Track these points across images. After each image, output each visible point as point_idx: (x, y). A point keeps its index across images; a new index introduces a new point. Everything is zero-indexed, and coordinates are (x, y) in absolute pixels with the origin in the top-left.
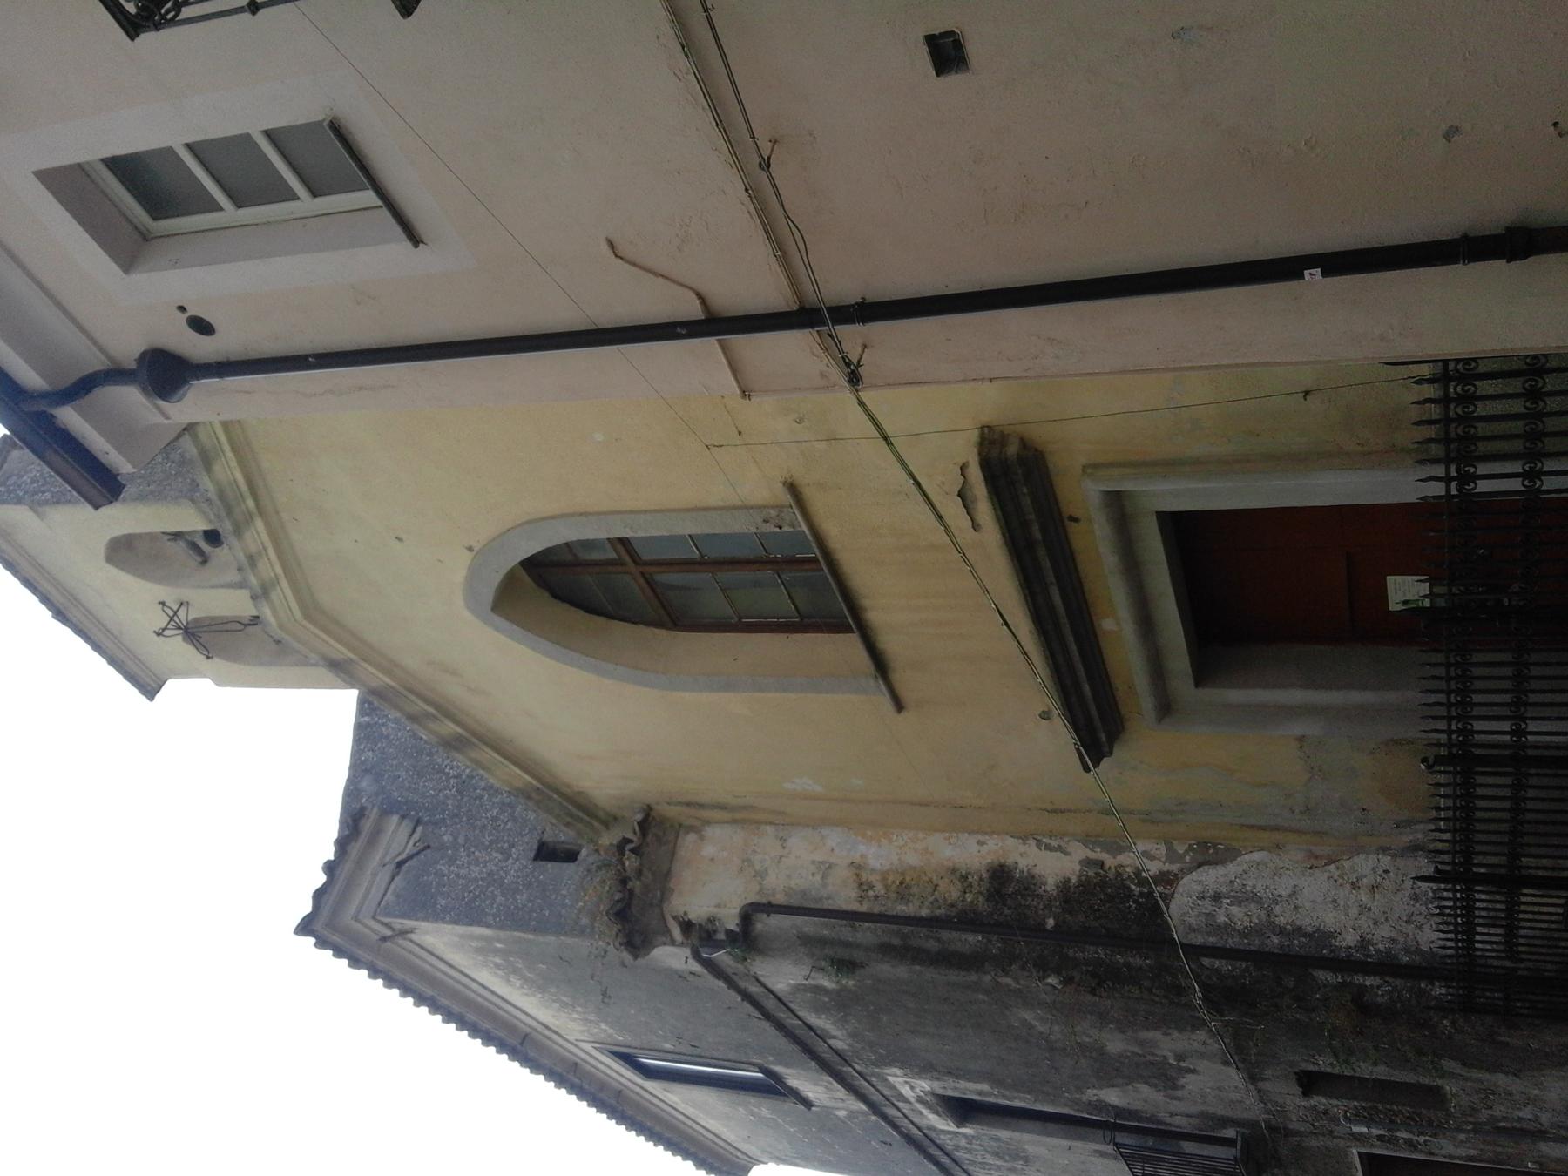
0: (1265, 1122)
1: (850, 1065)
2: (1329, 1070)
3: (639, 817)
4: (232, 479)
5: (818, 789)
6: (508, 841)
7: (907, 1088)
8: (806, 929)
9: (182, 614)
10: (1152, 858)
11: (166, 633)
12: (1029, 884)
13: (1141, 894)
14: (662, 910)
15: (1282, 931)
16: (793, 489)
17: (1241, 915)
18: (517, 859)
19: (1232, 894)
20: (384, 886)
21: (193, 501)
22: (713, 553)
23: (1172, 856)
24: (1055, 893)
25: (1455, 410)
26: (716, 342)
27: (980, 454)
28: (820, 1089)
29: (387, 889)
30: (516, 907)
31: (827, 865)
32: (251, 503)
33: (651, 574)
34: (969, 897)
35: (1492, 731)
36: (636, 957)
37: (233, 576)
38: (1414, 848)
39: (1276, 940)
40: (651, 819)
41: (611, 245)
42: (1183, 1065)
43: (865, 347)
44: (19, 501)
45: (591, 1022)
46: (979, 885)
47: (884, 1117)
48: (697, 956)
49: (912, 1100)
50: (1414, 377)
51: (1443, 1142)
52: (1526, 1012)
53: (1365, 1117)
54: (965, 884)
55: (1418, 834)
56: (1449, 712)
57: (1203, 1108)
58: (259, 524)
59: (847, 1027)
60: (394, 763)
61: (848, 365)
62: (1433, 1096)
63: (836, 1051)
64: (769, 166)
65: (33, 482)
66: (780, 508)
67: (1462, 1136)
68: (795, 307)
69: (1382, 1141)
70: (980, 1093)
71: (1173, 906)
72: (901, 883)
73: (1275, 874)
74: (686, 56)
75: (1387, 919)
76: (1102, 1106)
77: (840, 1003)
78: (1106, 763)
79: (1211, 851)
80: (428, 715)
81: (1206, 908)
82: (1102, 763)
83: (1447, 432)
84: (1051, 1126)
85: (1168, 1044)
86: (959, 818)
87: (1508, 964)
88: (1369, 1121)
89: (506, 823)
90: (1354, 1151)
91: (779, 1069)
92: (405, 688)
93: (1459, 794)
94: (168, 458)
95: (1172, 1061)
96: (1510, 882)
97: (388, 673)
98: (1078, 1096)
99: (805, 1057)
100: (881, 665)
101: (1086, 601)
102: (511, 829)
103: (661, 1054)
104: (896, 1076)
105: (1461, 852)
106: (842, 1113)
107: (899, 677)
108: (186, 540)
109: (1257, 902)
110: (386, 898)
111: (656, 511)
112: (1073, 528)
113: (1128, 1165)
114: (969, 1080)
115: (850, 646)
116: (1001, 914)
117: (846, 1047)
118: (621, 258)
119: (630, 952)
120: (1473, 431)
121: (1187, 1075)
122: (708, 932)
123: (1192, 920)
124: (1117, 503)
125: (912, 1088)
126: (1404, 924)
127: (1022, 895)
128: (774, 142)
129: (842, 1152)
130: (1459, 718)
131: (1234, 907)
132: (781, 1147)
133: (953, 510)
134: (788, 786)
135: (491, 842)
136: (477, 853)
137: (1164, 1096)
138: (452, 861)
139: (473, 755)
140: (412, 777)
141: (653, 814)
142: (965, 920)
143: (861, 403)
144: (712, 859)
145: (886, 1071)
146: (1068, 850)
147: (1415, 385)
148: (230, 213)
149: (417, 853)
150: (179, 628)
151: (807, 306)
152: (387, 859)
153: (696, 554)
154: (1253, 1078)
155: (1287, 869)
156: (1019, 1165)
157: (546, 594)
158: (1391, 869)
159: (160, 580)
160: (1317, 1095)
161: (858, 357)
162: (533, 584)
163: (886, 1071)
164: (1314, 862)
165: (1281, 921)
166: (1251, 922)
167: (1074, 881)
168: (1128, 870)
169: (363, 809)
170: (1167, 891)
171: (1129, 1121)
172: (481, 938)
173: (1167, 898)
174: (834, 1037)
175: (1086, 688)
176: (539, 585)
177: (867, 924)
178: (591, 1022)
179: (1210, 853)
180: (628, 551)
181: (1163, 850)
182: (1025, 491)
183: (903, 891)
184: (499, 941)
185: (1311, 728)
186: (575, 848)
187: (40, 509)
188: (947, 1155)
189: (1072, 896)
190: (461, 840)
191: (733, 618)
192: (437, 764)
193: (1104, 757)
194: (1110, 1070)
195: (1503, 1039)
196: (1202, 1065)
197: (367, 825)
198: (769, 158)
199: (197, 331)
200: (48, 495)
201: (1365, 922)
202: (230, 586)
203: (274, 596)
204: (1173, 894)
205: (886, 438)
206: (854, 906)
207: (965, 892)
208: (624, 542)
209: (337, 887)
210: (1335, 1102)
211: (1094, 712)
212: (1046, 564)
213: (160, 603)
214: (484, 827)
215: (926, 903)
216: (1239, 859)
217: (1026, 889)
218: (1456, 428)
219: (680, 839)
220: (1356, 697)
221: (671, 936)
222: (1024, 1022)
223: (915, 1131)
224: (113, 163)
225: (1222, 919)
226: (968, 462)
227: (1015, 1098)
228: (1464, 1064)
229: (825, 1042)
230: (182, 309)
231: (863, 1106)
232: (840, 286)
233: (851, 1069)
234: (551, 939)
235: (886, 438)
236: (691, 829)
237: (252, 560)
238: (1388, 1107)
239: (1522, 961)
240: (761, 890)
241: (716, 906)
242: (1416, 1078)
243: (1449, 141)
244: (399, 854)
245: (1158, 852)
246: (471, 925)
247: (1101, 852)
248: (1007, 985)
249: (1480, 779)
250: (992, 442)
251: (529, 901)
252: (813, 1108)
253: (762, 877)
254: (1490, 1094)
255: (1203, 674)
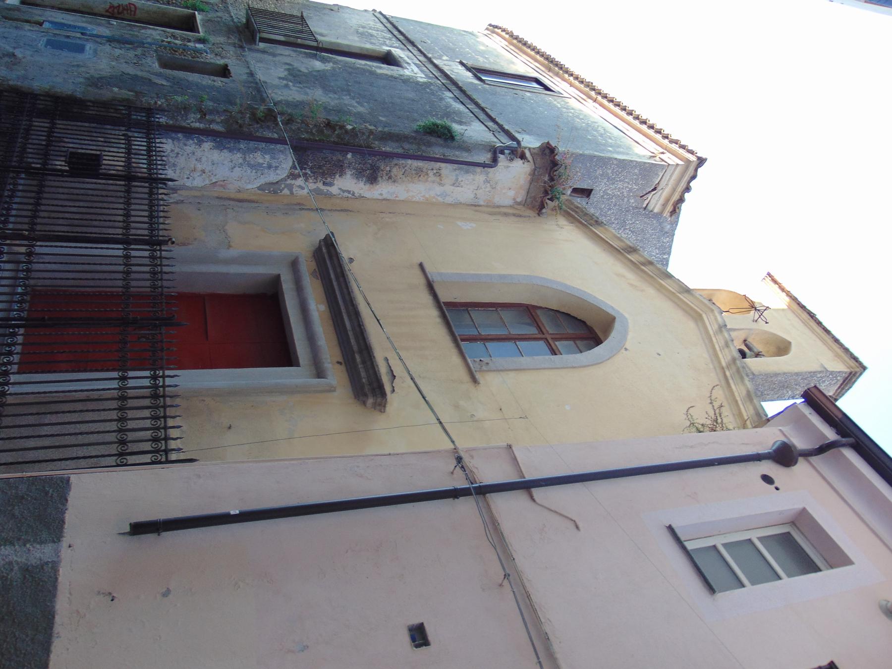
0: (245, 50)
1: (442, 83)
2: (215, 78)
3: (544, 211)
4: (737, 386)
5: (459, 223)
6: (604, 198)
7: (415, 71)
8: (467, 154)
9: (757, 316)
10: (300, 187)
11: (764, 308)
12: (359, 174)
13: (305, 169)
14: (535, 166)
15: (239, 149)
16: (475, 381)
17: (258, 158)
18: (600, 190)
19: (262, 169)
20: (663, 180)
21: (754, 374)
22: (510, 345)
23: (290, 188)
24: (347, 170)
25: (161, 434)
26: (526, 476)
27: (386, 400)
28: (456, 71)
29: (662, 178)
30: (602, 167)
31: (455, 185)
32: (728, 373)
33: (539, 333)
34: (388, 168)
35: (140, 253)
36: (548, 143)
37: (733, 334)
38: (175, 190)
39: (242, 146)
40: (539, 209)
41: (577, 527)
42: (285, 82)
43: (452, 473)
44: (832, 373)
45: (565, 108)
46: (383, 174)
47: (425, 56)
48: (518, 142)
49: (412, 64)
50: (182, 452)
51: (158, 37)
52: (121, 108)
53: (198, 52)
54: (389, 175)
55: (175, 197)
56: (161, 269)
57: (274, 59)
58: (724, 364)
59: (445, 103)
60: (653, 236)
61: (462, 467)
62: (165, 64)
63: (450, 91)
64: (505, 575)
65: (824, 381)
66: (481, 371)
67: (149, 40)
68: (488, 495)
69: (188, 39)
70: (380, 68)
71: (291, 164)
72: (420, 176)
73: (241, 178)
74: (546, 633)
75: (188, 154)
76: (324, 60)
77: (449, 114)
78: (323, 237)
79: (272, 189)
80: (643, 264)
81: (275, 162)
82: (324, 236)
83: (165, 422)
84: (347, 50)
85: (294, 94)
86: (390, 205)
87: (130, 134)
88: (196, 51)
89: (605, 207)
90: (201, 34)
91: (476, 82)
92: (655, 279)
93: (156, 225)
94: (762, 392)
95: (290, 84)
96: (129, 177)
97: (661, 285)
98: (335, 66)
99: (464, 88)
100: (430, 287)
101: (333, 320)
102: (602, 204)
103: (531, 90)
104: (421, 77)
105: (154, 194)
106: (445, 58)
107: (422, 281)
108: (753, 351)
109: (250, 164)
110: (663, 173)
111: (540, 369)
112: (340, 359)
113: (311, 30)
114: (387, 75)
115: (444, 297)
116: (373, 160)
117: (445, 92)
118: (572, 520)
119: (551, 145)
120: (153, 422)
121: (284, 76)
122: (513, 154)
123: (282, 156)
124: (320, 373)
125: (413, 71)
126: (180, 153)
127: (362, 169)
128: (501, 585)
129: (444, 38)
130: (156, 265)
131: (261, 162)
132: (473, 41)
133: (398, 370)
134: (474, 225)
135: (612, 198)
136: (619, 193)
137: (294, 65)
138: (630, 190)
139: (622, 244)
140: (646, 230)
141: (537, 212)
142: (389, 156)
143: (453, 442)
144: (510, 189)
145: (426, 80)
146: (339, 191)
147: (181, 447)
148: (754, 536)
149: (647, 194)
150: (759, 310)
151: (482, 496)
152: (661, 191)
153: (518, 343)
154: (251, 74)
155: (235, 180)
156: (361, 30)
157: (588, 323)
158: (186, 180)
159: (766, 332)
160: (220, 65)
161: (456, 468)
162: (594, 328)
163: (426, 80)
164: (223, 184)
165: (239, 155)
166: (254, 155)
167: (338, 176)
168: (311, 181)
169: (671, 216)
170: (293, 170)
171: (310, 53)
172: (618, 153)
173: (294, 167)
174: (450, 98)
175: (332, 276)
176: (592, 328)
177: (437, 156)
178: (565, 108)
179: (273, 188)
180: (550, 345)
181: (294, 190)
182: (364, 380)
183: (419, 172)
184: (610, 151)
185: (224, 254)
186: (573, 194)
187: (823, 369)
188: (394, 35)
189: (339, 169)
190: (626, 199)
191: (500, 310)
192: (634, 235)
193: (323, 240)
194: (320, 79)
195: (132, 93)
196: (276, 82)
197: (669, 208)
198: (505, 578)
199: (767, 476)
200: (819, 376)
201: (199, 153)
202: (735, 330)
203: (716, 327)
204: (290, 169)
205: (440, 423)
206: (443, 165)
207: (390, 171)
208: (554, 352)
209: (685, 179)
210: (212, 61)
211: (328, 262)
212: (353, 341)
213: (768, 323)
214: (615, 205)
215: (408, 166)
216: (259, 185)
217: (360, 172)
218: (161, 424)
219: (525, 199)
220: (203, 268)
221: (530, 152)
222: (362, 106)
223: (410, 48)
224: (817, 569)
225: (267, 157)
226: (391, 394)
227: (364, 65)
228: (150, 80)
229: (455, 96)
230: (777, 489)
231: (435, 61)
232: (466, 506)
233: (443, 81)
234: (586, 152)
235: (440, 423)
236: (519, 204)
237: (727, 345)
238: (186, 58)
239: (123, 135)
240: (487, 174)
241: (510, 166)
242: (173, 73)
243: (168, 588)
244: (655, 194)
245: (297, 189)
246: (624, 160)
247: (324, 190)
248: (370, 125)
249: (146, 232)
250: (380, 405)
251: (596, 170)
252: (459, 61)
253: (487, 180)
254: (136, 63)
255: (276, 281)
